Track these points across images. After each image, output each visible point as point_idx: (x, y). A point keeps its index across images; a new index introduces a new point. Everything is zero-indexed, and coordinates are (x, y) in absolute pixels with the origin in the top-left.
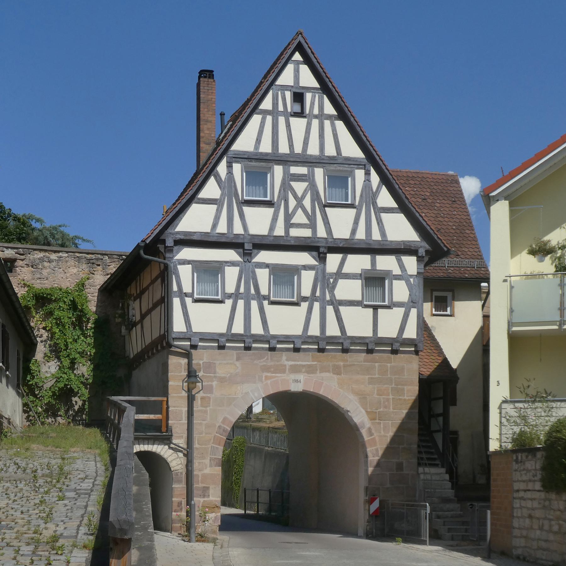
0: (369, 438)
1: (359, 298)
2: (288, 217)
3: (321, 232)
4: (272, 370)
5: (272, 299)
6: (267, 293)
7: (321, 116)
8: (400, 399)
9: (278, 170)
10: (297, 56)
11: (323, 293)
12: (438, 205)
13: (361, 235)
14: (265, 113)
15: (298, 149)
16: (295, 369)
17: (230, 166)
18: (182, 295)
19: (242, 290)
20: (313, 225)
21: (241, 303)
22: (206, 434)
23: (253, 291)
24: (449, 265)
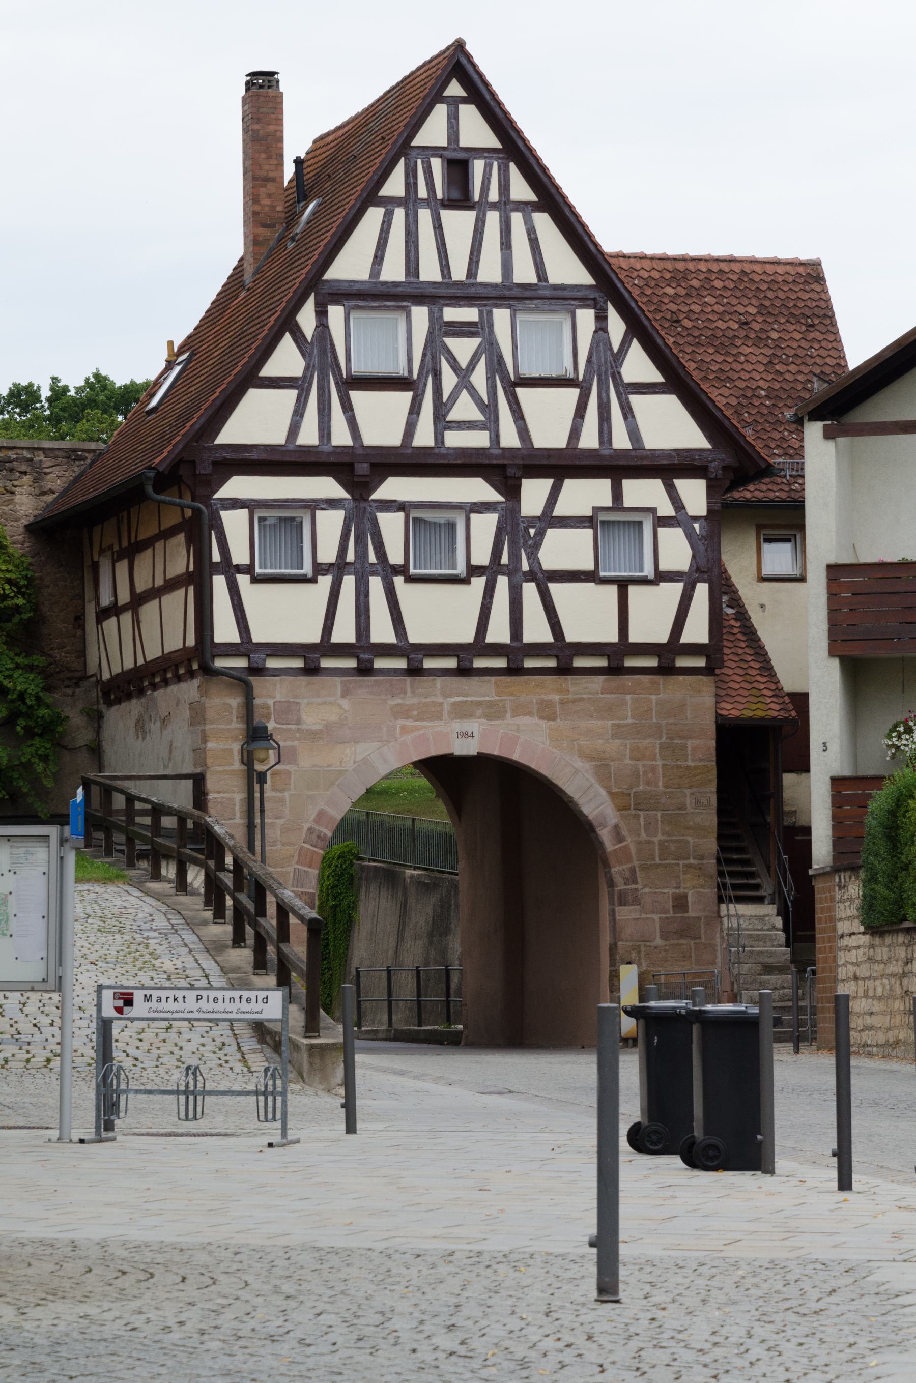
0: (617, 847)
1: (589, 566)
2: (441, 409)
3: (510, 438)
4: (415, 713)
5: (412, 571)
6: (246, 561)
7: (506, 205)
8: (678, 767)
9: (420, 314)
10: (455, 89)
11: (515, 557)
12: (775, 335)
13: (589, 439)
14: (389, 203)
15: (459, 273)
16: (462, 712)
17: (321, 314)
18: (230, 570)
19: (351, 557)
20: (491, 423)
21: (349, 583)
22: (283, 845)
23: (372, 558)
24: (794, 473)
